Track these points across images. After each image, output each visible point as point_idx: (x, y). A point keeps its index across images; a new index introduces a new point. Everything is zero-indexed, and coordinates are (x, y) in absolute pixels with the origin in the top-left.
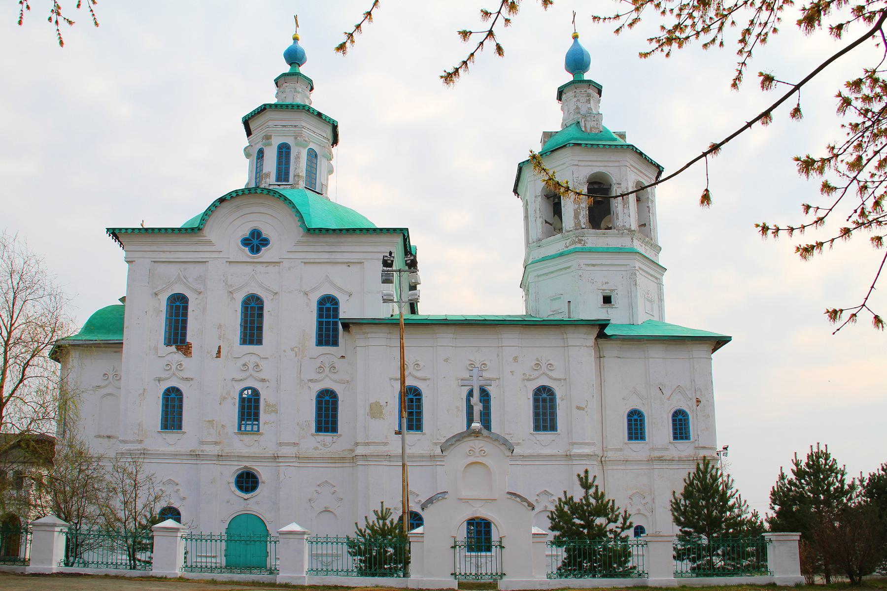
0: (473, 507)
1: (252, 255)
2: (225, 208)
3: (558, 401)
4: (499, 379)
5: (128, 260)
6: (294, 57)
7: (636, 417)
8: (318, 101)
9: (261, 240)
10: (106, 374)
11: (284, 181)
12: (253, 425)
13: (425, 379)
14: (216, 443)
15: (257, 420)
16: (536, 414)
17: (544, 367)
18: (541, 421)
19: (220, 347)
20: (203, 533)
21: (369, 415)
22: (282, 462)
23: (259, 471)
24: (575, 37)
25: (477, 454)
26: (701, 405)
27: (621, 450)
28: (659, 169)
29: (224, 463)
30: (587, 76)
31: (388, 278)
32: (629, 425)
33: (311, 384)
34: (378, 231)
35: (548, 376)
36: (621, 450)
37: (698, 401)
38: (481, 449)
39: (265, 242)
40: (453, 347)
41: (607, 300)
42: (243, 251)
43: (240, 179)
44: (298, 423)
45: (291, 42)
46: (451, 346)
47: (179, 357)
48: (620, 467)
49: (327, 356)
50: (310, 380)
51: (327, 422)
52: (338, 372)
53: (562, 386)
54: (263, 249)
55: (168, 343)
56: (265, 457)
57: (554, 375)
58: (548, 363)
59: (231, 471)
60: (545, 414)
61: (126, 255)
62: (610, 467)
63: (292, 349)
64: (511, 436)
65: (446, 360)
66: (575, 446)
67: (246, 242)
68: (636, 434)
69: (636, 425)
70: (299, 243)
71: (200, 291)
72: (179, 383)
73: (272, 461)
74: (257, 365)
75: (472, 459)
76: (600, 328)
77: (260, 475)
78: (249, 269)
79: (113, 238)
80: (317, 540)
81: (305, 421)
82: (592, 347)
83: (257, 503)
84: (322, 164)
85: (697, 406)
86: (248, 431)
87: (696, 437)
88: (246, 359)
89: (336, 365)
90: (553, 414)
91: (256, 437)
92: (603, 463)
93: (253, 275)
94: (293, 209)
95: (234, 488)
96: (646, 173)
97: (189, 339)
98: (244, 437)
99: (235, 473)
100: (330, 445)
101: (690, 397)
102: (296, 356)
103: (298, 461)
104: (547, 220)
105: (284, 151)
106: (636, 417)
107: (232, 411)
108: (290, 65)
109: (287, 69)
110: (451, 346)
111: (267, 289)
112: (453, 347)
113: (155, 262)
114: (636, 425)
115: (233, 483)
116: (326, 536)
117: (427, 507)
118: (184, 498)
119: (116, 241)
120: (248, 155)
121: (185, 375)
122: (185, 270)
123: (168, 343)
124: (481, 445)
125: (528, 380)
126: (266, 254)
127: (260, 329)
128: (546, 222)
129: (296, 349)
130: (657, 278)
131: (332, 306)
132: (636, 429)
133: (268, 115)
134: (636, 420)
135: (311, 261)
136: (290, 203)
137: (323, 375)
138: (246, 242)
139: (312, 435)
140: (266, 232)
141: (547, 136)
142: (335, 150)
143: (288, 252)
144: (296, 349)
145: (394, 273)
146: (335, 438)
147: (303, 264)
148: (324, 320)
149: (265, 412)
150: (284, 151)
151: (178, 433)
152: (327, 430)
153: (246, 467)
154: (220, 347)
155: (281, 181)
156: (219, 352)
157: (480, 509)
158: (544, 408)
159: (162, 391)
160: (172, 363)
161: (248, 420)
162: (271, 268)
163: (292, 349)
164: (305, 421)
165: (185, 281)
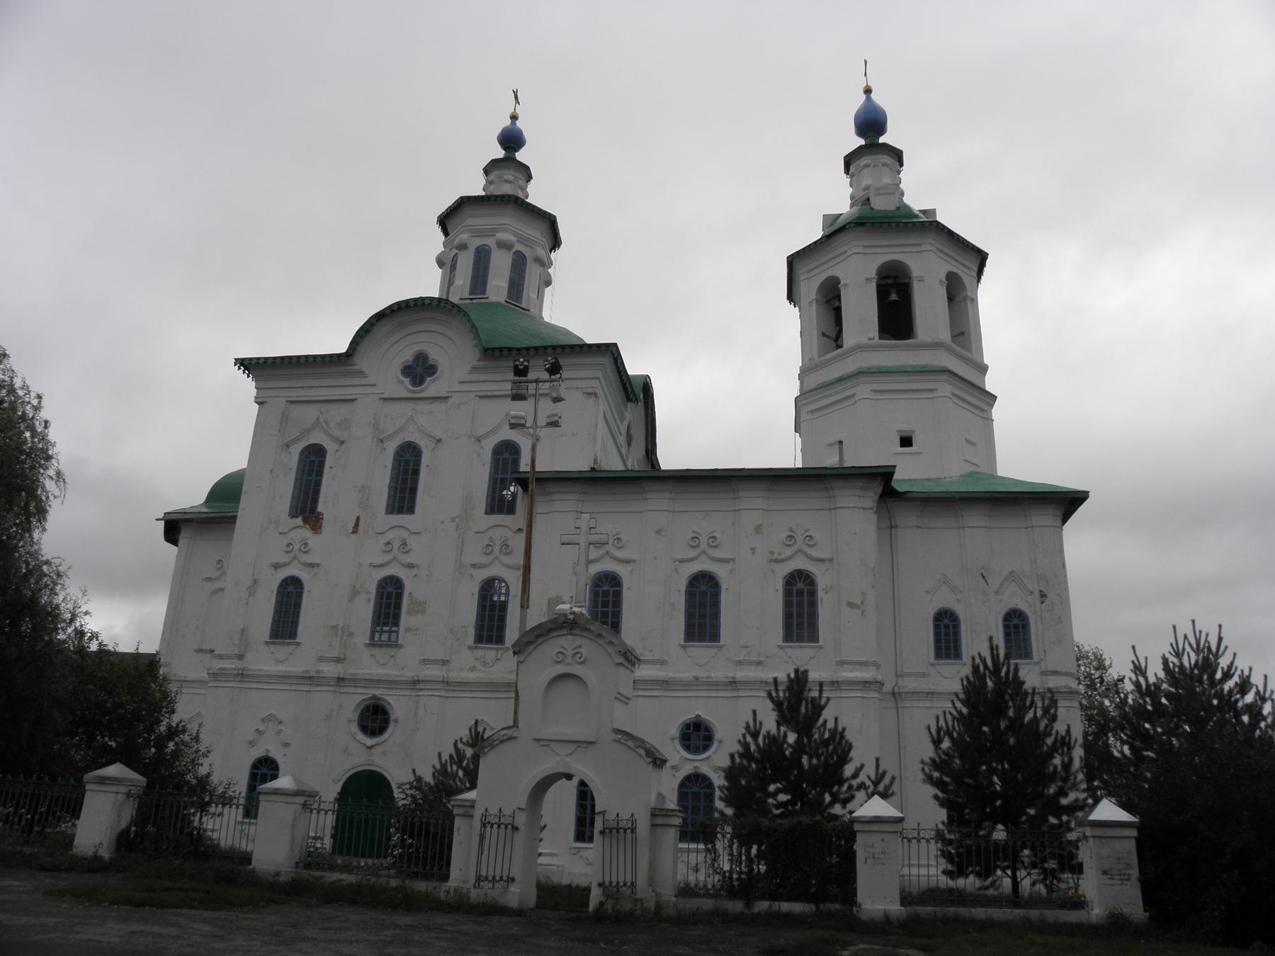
0: (557, 754)
1: (413, 389)
2: (381, 329)
3: (820, 593)
4: (734, 560)
5: (259, 400)
6: (511, 140)
7: (946, 621)
8: (537, 195)
9: (418, 365)
10: (221, 561)
11: (480, 294)
12: (391, 632)
13: (627, 562)
14: (339, 660)
15: (397, 624)
16: (788, 616)
17: (800, 540)
18: (795, 627)
19: (358, 519)
20: (922, 826)
21: (546, 615)
22: (424, 689)
23: (391, 702)
24: (868, 91)
25: (569, 660)
26: (1048, 601)
27: (924, 675)
28: (981, 255)
29: (343, 690)
30: (882, 140)
31: (519, 392)
32: (937, 634)
33: (472, 571)
34: (586, 349)
35: (805, 554)
36: (924, 675)
37: (1043, 596)
38: (575, 651)
39: (431, 370)
40: (669, 511)
41: (906, 441)
42: (402, 383)
43: (429, 284)
44: (452, 630)
45: (508, 122)
46: (666, 511)
47: (306, 533)
48: (922, 704)
49: (500, 529)
50: (474, 566)
51: (490, 629)
52: (511, 552)
53: (828, 569)
54: (429, 379)
55: (293, 515)
56: (400, 682)
57: (814, 553)
58: (805, 535)
59: (352, 702)
60: (800, 615)
61: (257, 394)
62: (908, 704)
63: (453, 520)
64: (749, 649)
65: (659, 532)
66: (845, 666)
67: (407, 370)
68: (948, 648)
69: (947, 634)
70: (474, 369)
71: (342, 439)
72: (301, 570)
73: (409, 687)
74: (405, 544)
75: (561, 669)
76: (884, 476)
77: (392, 708)
78: (407, 408)
79: (244, 372)
80: (919, 834)
81: (462, 627)
82: (871, 509)
83: (385, 753)
84: (532, 271)
85: (1042, 603)
86: (383, 641)
87: (1042, 654)
88: (391, 536)
89: (510, 543)
90: (813, 615)
91: (392, 651)
92: (897, 695)
93: (412, 416)
94: (468, 324)
95: (355, 729)
96: (964, 262)
97: (320, 508)
98: (377, 651)
99: (358, 705)
100: (491, 664)
101: (1031, 589)
102: (457, 529)
103: (446, 688)
104: (824, 331)
105: (482, 257)
106: (946, 621)
107: (365, 611)
108: (505, 149)
109: (500, 153)
110: (666, 511)
111: (429, 435)
112: (669, 511)
113: (292, 402)
114: (947, 634)
115: (354, 721)
116: (916, 827)
117: (483, 753)
118: (286, 745)
119: (248, 377)
120: (440, 262)
121: (309, 559)
122: (327, 411)
123: (293, 515)
124: (578, 643)
125: (777, 561)
126: (432, 387)
127: (414, 491)
128: (824, 335)
129: (457, 519)
130: (983, 410)
131: (511, 457)
132: (947, 641)
133: (468, 210)
134: (947, 627)
135: (489, 393)
136: (465, 315)
137: (491, 558)
138: (407, 370)
139: (470, 648)
140: (435, 355)
141: (829, 220)
142: (553, 255)
143: (460, 382)
144: (457, 519)
145: (529, 384)
146: (500, 652)
147: (478, 398)
148: (499, 476)
149: (408, 613)
150: (482, 257)
151: (290, 644)
152: (489, 640)
153: (374, 697)
154: (358, 519)
155: (475, 295)
156: (357, 525)
157: (568, 759)
158: (800, 605)
159: (278, 582)
160: (295, 543)
161: (385, 624)
162: (437, 407)
163: (453, 520)
164: (462, 627)
165: (325, 426)
